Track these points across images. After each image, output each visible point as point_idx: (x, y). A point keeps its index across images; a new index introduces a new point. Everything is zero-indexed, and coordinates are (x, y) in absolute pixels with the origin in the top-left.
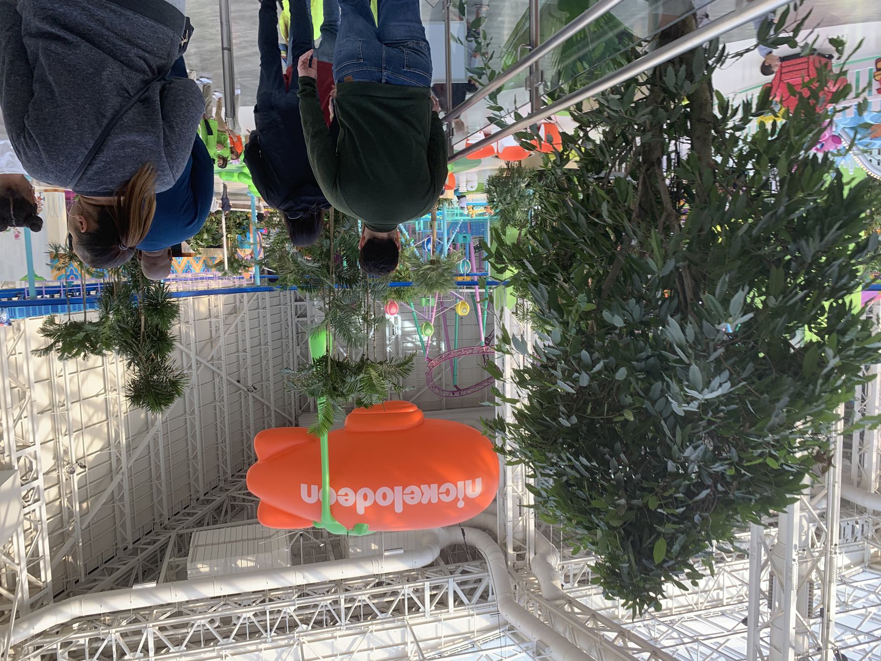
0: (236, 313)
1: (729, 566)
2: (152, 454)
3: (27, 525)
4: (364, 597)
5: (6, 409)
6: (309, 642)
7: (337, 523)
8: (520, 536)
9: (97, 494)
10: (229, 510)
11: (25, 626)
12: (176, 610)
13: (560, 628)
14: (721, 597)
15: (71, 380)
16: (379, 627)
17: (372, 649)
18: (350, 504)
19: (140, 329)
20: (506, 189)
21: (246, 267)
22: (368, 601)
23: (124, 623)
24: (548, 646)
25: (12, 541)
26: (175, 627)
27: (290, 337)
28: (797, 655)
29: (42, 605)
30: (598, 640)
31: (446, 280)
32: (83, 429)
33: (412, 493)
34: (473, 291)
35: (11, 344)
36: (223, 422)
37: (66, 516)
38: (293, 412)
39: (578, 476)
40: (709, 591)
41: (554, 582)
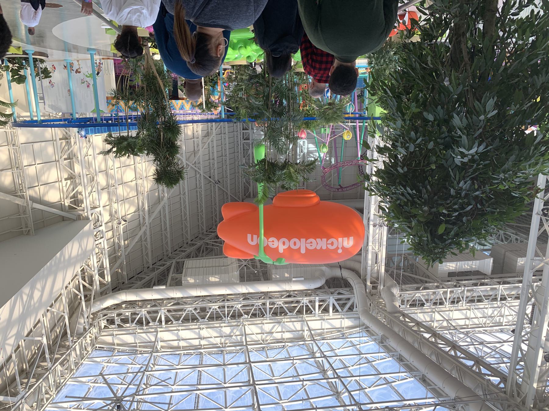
0: (208, 136)
1: (509, 303)
2: (162, 216)
3: (97, 250)
4: (280, 303)
5: (85, 186)
6: (249, 325)
7: (267, 257)
8: (375, 275)
9: (133, 237)
10: (205, 250)
11: (98, 303)
12: (176, 302)
13: (396, 330)
14: (501, 321)
15: (117, 172)
16: (288, 320)
17: (284, 332)
18: (275, 246)
19: (160, 141)
20: (381, 56)
21: (215, 107)
22: (282, 305)
23: (149, 306)
24: (388, 338)
25: (90, 259)
26: (175, 311)
27: (240, 152)
28: (544, 352)
29: (106, 294)
30: (419, 337)
31: (338, 116)
32: (124, 200)
33: (311, 243)
34: (355, 124)
35: (85, 150)
36: (201, 200)
37: (117, 248)
38: (241, 197)
39: (406, 200)
40: (494, 317)
41: (395, 303)
